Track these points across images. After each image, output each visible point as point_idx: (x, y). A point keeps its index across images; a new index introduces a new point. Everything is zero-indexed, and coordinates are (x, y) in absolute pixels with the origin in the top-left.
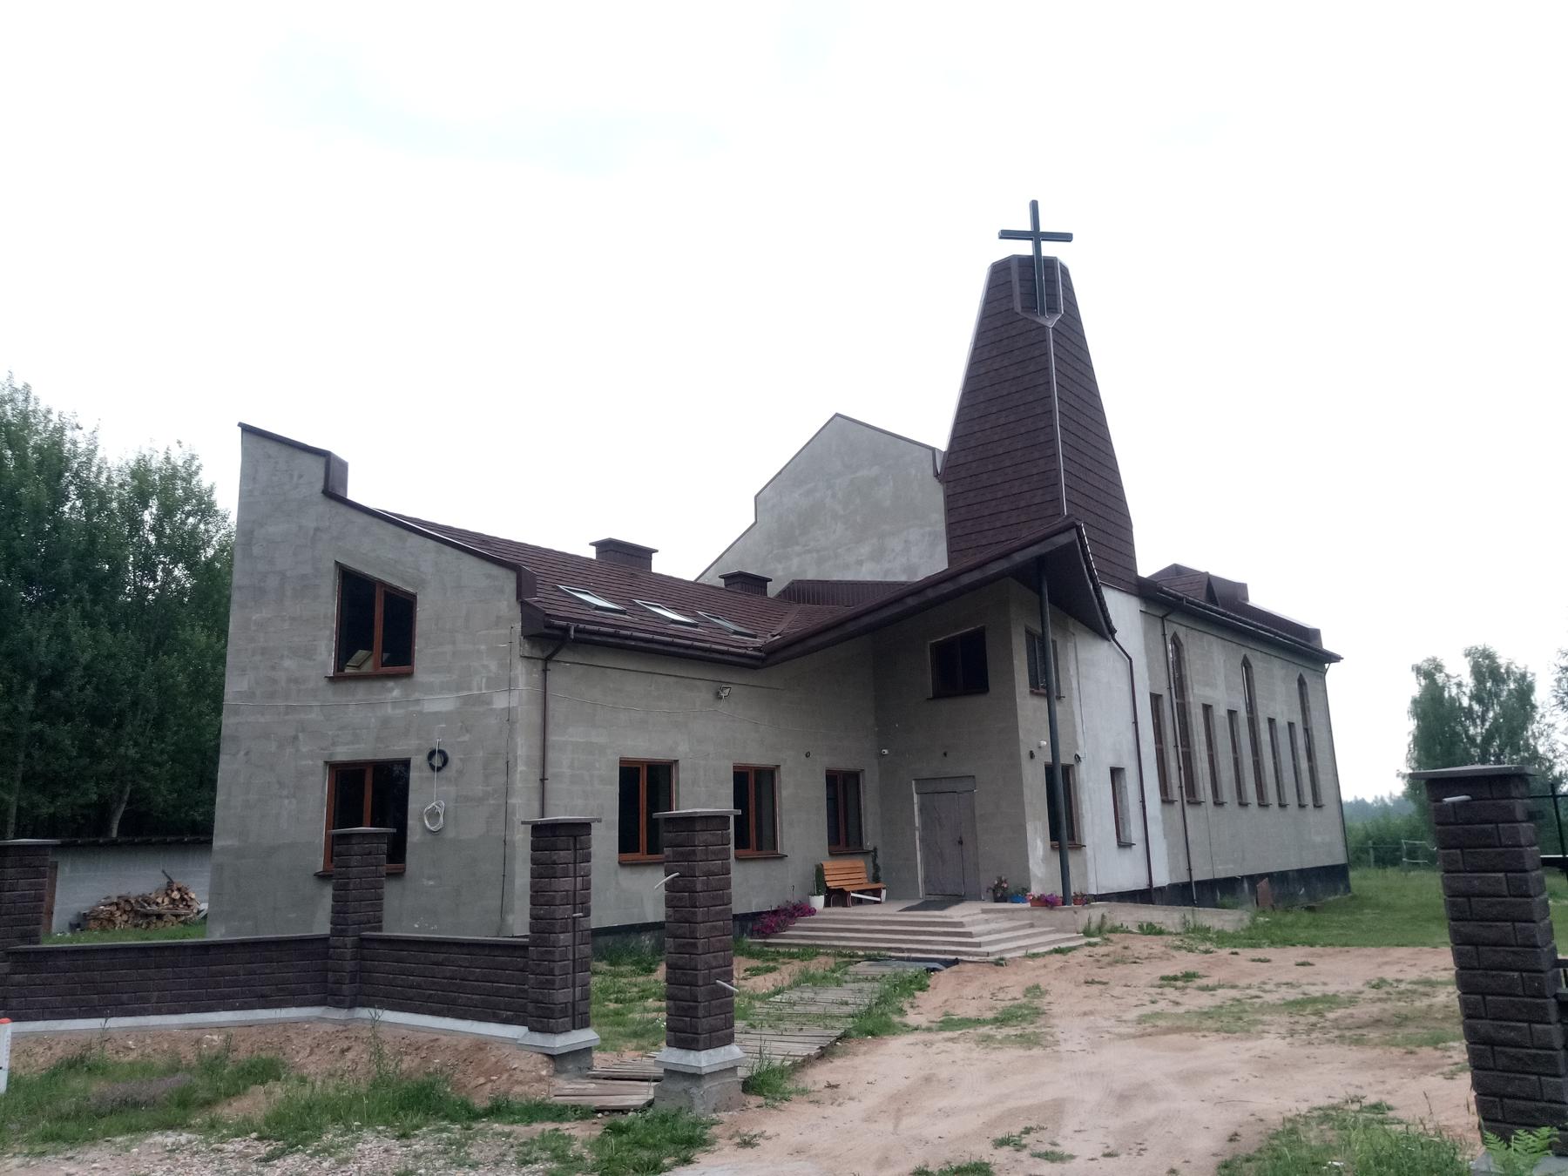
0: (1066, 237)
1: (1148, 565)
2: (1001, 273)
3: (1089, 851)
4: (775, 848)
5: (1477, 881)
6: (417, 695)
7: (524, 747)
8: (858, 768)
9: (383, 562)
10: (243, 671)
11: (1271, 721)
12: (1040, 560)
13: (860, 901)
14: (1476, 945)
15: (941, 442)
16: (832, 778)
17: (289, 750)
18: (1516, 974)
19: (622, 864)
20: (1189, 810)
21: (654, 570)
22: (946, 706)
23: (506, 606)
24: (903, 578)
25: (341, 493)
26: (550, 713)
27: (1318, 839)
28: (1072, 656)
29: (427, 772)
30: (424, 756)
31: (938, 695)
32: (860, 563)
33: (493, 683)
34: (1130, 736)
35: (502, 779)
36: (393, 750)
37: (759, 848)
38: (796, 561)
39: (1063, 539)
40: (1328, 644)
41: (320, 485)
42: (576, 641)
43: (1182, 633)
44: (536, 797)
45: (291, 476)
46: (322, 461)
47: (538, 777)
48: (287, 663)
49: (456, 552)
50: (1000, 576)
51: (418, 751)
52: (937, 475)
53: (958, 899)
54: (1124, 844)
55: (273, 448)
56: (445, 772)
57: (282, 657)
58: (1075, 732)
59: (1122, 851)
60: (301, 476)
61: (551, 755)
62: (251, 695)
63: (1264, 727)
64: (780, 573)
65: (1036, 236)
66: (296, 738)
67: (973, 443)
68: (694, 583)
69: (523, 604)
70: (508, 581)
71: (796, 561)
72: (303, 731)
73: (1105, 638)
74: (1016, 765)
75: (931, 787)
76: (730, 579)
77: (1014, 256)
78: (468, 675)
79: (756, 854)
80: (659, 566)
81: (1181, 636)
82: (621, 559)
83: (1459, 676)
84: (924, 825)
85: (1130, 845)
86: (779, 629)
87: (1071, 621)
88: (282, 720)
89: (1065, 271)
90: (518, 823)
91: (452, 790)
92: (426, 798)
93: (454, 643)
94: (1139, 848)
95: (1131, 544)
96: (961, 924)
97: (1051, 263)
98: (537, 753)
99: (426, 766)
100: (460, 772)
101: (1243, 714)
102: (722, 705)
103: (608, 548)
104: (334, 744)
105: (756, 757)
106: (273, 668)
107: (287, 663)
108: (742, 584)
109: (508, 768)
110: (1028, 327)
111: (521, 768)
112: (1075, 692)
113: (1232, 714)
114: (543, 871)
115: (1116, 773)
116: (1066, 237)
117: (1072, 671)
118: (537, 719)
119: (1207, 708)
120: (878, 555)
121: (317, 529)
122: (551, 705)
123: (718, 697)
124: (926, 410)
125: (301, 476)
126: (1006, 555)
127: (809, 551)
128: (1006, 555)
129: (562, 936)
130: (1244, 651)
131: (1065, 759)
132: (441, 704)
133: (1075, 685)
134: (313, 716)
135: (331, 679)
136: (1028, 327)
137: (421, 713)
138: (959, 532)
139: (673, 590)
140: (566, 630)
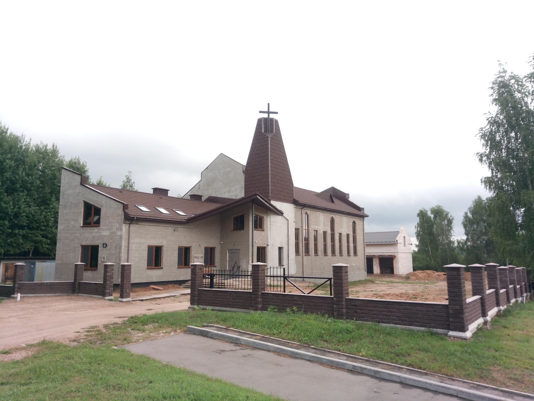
0: (277, 113)
7: (124, 243)
9: (95, 200)
15: (244, 163)
16: (206, 249)
20: (305, 258)
21: (169, 195)
23: (120, 212)
24: (234, 198)
26: (130, 236)
27: (354, 265)
29: (103, 248)
31: (234, 230)
32: (225, 193)
33: (117, 229)
34: (286, 239)
39: (254, 197)
40: (366, 212)
41: (80, 182)
43: (309, 212)
48: (72, 223)
61: (130, 245)
65: (269, 112)
69: (125, 212)
70: (121, 206)
71: (210, 191)
75: (232, 252)
79: (154, 267)
80: (170, 194)
81: (308, 213)
84: (229, 261)
87: (269, 212)
88: (71, 234)
90: (354, 219)
92: (102, 254)
97: (272, 120)
98: (127, 245)
103: (156, 190)
105: (185, 244)
108: (195, 198)
109: (120, 248)
110: (267, 135)
111: (123, 248)
112: (269, 229)
114: (106, 272)
115: (280, 249)
116: (277, 113)
118: (127, 237)
122: (131, 234)
123: (174, 230)
124: (242, 156)
132: (106, 233)
133: (269, 227)
136: (267, 135)
140: (134, 218)
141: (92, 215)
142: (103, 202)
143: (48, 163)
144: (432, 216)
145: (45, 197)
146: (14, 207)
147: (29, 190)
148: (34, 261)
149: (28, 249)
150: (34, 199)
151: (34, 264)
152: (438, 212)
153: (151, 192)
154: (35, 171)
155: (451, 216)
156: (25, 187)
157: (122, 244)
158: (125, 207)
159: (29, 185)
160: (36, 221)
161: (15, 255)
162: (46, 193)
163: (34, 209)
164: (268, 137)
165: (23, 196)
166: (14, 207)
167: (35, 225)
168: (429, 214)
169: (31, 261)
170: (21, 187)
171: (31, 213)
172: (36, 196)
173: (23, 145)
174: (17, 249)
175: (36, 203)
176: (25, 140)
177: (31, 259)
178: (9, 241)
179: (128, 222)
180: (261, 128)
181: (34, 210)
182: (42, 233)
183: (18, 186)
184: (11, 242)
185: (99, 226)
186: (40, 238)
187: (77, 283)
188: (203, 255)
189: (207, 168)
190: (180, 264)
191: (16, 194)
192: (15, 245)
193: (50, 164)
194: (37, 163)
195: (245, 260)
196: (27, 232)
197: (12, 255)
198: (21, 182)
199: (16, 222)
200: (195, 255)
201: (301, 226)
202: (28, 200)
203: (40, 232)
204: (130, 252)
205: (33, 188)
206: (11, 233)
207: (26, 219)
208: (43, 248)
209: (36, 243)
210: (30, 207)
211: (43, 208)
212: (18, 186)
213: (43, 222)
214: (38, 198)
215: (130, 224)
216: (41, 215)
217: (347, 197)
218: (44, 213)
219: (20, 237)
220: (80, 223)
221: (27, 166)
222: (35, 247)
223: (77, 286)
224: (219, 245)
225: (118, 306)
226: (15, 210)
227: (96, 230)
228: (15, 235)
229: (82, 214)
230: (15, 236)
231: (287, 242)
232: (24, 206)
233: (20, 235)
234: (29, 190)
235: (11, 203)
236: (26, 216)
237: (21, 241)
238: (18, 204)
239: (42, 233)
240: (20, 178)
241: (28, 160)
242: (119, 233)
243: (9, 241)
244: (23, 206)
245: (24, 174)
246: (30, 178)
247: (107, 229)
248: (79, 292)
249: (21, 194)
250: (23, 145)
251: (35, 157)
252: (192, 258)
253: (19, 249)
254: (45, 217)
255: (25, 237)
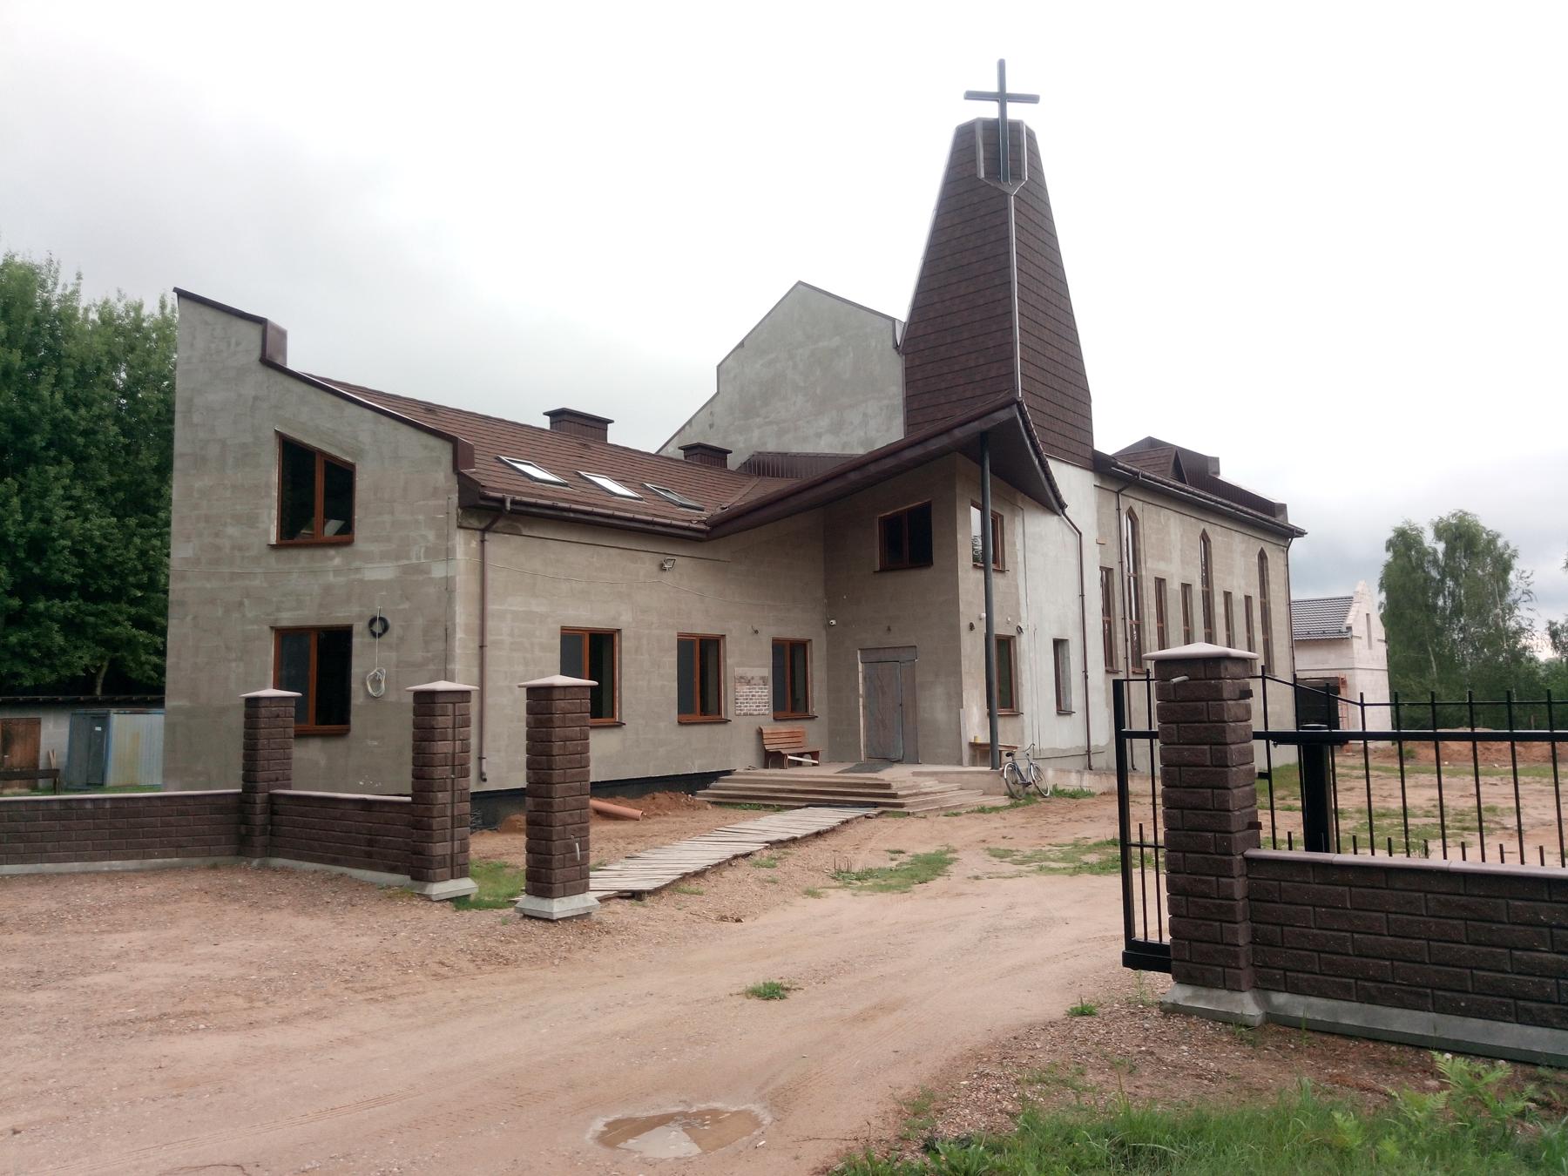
0: (1033, 99)
1: (1109, 438)
2: (965, 138)
3: (1026, 718)
4: (719, 713)
5: (1187, 752)
6: (357, 564)
8: (807, 638)
9: (324, 430)
10: (188, 539)
11: (1227, 595)
12: (984, 436)
13: (799, 764)
14: (1182, 808)
16: (778, 646)
17: (236, 615)
18: (1210, 835)
19: (680, 723)
22: (894, 581)
23: (442, 477)
25: (279, 361)
28: (1019, 530)
29: (368, 639)
30: (366, 623)
31: (885, 568)
32: (819, 435)
33: (432, 553)
34: (1076, 608)
35: (440, 645)
36: (337, 616)
37: (793, 710)
38: (756, 433)
39: (1003, 415)
40: (1293, 519)
41: (257, 354)
42: (512, 512)
43: (1138, 507)
44: (475, 662)
45: (229, 344)
46: (254, 332)
47: (476, 645)
48: (231, 530)
49: (393, 422)
50: (943, 453)
51: (360, 617)
52: (896, 347)
53: (891, 761)
54: (1062, 710)
55: (209, 314)
56: (385, 637)
57: (225, 525)
58: (1018, 603)
59: (1062, 718)
60: (238, 344)
61: (490, 624)
62: (197, 561)
63: (1219, 601)
64: (741, 445)
65: (1002, 97)
66: (241, 604)
67: (932, 315)
68: (656, 456)
69: (461, 477)
70: (444, 452)
71: (756, 433)
72: (248, 596)
73: (1056, 513)
74: (956, 638)
75: (874, 657)
76: (689, 450)
77: (979, 120)
78: (402, 542)
80: (614, 436)
81: (1136, 511)
82: (578, 429)
83: (1512, 546)
84: (868, 695)
85: (1070, 713)
86: (732, 500)
87: (1020, 496)
89: (1031, 136)
91: (393, 656)
92: (369, 665)
93: (392, 513)
94: (1079, 716)
95: (1087, 418)
96: (888, 786)
97: (1016, 127)
99: (367, 632)
100: (401, 639)
101: (1198, 587)
102: (667, 578)
104: (278, 610)
106: (217, 535)
107: (231, 530)
108: (702, 455)
109: (448, 635)
110: (990, 204)
111: (460, 634)
112: (1021, 566)
113: (1186, 587)
114: (424, 734)
115: (1059, 644)
116: (1033, 99)
117: (1019, 545)
118: (475, 588)
119: (1160, 583)
120: (836, 428)
121: (256, 398)
122: (490, 575)
123: (662, 568)
124: (890, 288)
125: (238, 344)
126: (948, 431)
127: (770, 423)
128: (948, 431)
129: (440, 795)
130: (1203, 526)
131: (1000, 629)
132: (380, 572)
133: (1020, 558)
134: (257, 582)
135: (273, 547)
136: (990, 204)
137: (361, 581)
138: (915, 406)
139: (628, 463)
140: (502, 501)
141: (316, 494)
142: (365, 438)
143: (145, 364)
144: (1441, 547)
145: (139, 485)
146: (28, 518)
147: (80, 458)
148: (104, 710)
149: (86, 669)
150: (101, 492)
151: (104, 721)
152: (1463, 537)
153: (545, 423)
154: (100, 390)
155: (1507, 546)
156: (61, 445)
157: (453, 618)
158: (461, 455)
159: (81, 440)
160: (109, 569)
161: (37, 689)
162: (142, 470)
163: (100, 523)
164: (1005, 195)
165: (58, 476)
166: (28, 518)
167: (107, 584)
168: (1429, 540)
169: (96, 710)
170: (50, 444)
171: (89, 539)
172: (107, 480)
173: (54, 297)
174: (45, 671)
175: (108, 506)
176: (61, 282)
177: (96, 703)
178: (13, 639)
179: (476, 524)
180: (974, 161)
181: (100, 527)
182: (133, 611)
183: (39, 440)
184: (22, 644)
185: (349, 543)
186: (126, 630)
187: (260, 797)
188: (767, 672)
189: (741, 345)
190: (684, 706)
191: (31, 470)
192: (35, 654)
193: (154, 367)
194: (105, 360)
195: (939, 690)
196: (77, 608)
197: (25, 691)
198: (48, 427)
199: (37, 571)
200: (739, 671)
201: (1116, 559)
202: (77, 492)
203: (124, 606)
204: (490, 653)
205: (93, 451)
206: (22, 610)
207: (75, 560)
208: (142, 664)
209: (116, 650)
210: (86, 519)
211: (132, 522)
212: (39, 440)
213: (135, 572)
214: (116, 487)
215: (484, 531)
216: (126, 547)
217: (1211, 469)
218: (137, 540)
219: (56, 627)
220: (267, 532)
221: (70, 371)
222: (113, 662)
223: (259, 819)
224: (824, 633)
225: (534, 960)
226: (32, 526)
227: (336, 558)
228: (37, 618)
229: (275, 494)
230: (39, 624)
231: (1078, 619)
232: (63, 513)
233: (52, 619)
234: (80, 458)
235: (15, 501)
236: (74, 552)
237: (59, 639)
238: (41, 508)
239: (133, 611)
240: (43, 413)
241: (69, 347)
242: (438, 571)
243: (13, 639)
244: (59, 514)
245: (58, 396)
246: (83, 411)
247: (384, 556)
248: (272, 850)
249: (52, 471)
250: (54, 297)
251: (96, 338)
252: (730, 684)
253: (53, 668)
254: (143, 553)
255: (71, 626)
